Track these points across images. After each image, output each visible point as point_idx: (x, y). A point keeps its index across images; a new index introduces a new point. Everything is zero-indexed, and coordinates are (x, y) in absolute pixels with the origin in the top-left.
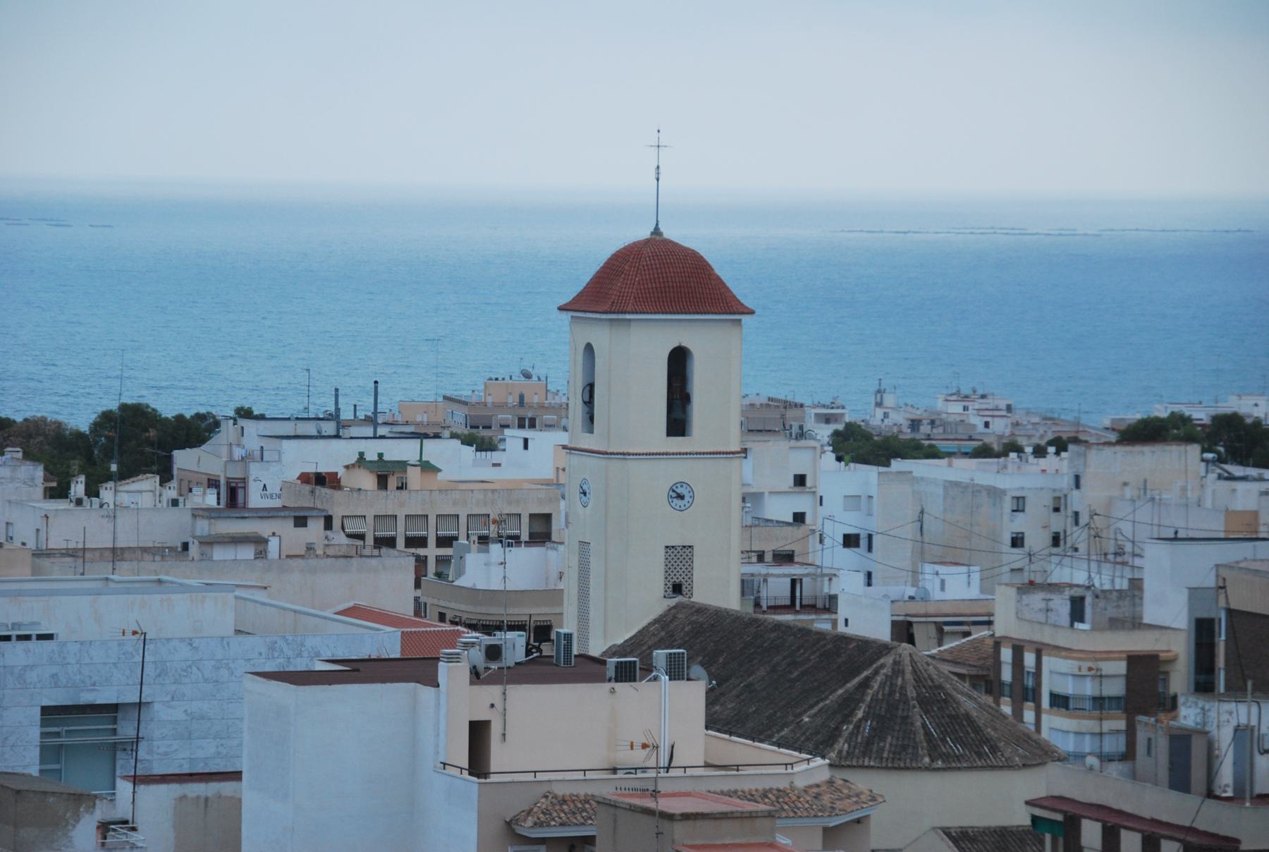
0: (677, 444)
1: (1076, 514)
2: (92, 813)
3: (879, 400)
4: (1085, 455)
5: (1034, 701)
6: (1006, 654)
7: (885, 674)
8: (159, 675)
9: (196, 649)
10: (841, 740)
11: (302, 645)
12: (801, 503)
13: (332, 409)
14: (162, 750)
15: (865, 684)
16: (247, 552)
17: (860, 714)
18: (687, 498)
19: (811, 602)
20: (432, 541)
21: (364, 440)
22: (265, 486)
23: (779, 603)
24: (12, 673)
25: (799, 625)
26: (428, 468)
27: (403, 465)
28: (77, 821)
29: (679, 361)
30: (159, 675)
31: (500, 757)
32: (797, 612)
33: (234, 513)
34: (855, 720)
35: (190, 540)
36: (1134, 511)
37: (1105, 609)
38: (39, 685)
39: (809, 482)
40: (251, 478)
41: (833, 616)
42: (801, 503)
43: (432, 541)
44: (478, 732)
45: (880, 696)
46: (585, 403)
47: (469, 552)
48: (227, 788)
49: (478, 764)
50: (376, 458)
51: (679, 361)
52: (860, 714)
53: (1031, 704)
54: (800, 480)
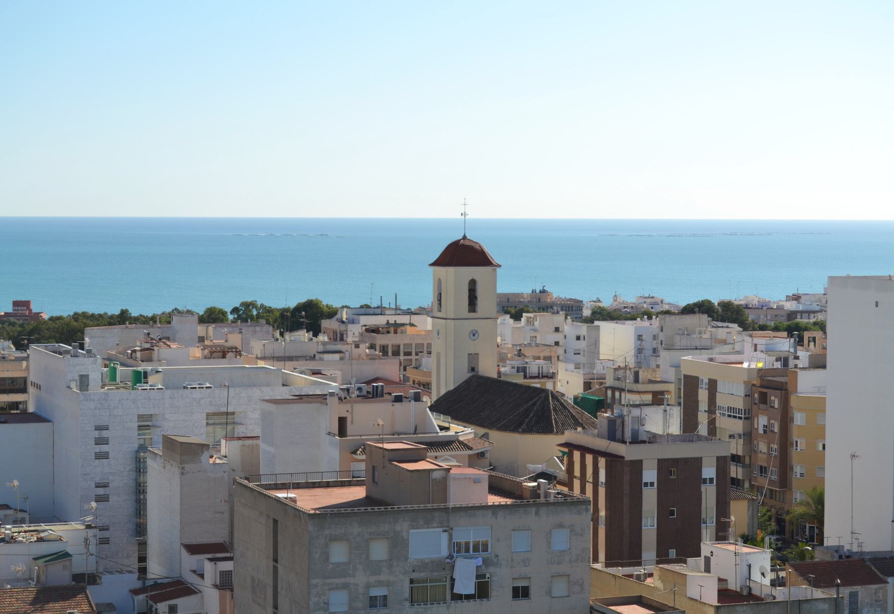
0: (472, 315)
1: (662, 341)
2: (208, 451)
3: (615, 299)
4: (665, 319)
5: (611, 409)
6: (609, 393)
7: (542, 400)
8: (249, 401)
9: (263, 392)
10: (524, 425)
11: (302, 390)
12: (558, 337)
13: (380, 304)
14: (251, 429)
15: (534, 404)
16: (337, 357)
17: (531, 415)
18: (474, 337)
19: (546, 375)
20: (414, 353)
21: (469, 318)
22: (354, 333)
23: (534, 375)
24: (195, 401)
25: (527, 384)
26: (412, 325)
27: (403, 325)
28: (203, 453)
29: (473, 284)
30: (249, 401)
31: (350, 429)
32: (541, 379)
33: (342, 342)
34: (530, 417)
35: (316, 353)
36: (681, 340)
37: (647, 376)
38: (205, 405)
39: (560, 330)
40: (349, 330)
41: (554, 380)
42: (558, 337)
43: (414, 353)
44: (342, 421)
45: (539, 408)
46: (438, 300)
47: (424, 357)
48: (255, 442)
49: (342, 432)
50: (394, 322)
51: (473, 284)
52: (531, 415)
53: (610, 410)
54: (557, 330)
